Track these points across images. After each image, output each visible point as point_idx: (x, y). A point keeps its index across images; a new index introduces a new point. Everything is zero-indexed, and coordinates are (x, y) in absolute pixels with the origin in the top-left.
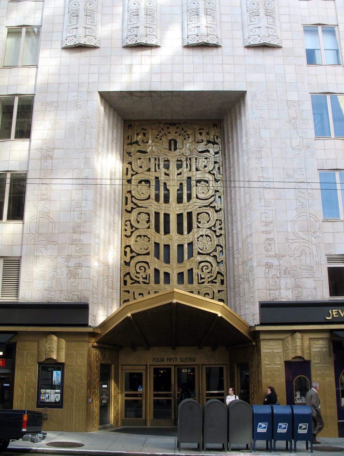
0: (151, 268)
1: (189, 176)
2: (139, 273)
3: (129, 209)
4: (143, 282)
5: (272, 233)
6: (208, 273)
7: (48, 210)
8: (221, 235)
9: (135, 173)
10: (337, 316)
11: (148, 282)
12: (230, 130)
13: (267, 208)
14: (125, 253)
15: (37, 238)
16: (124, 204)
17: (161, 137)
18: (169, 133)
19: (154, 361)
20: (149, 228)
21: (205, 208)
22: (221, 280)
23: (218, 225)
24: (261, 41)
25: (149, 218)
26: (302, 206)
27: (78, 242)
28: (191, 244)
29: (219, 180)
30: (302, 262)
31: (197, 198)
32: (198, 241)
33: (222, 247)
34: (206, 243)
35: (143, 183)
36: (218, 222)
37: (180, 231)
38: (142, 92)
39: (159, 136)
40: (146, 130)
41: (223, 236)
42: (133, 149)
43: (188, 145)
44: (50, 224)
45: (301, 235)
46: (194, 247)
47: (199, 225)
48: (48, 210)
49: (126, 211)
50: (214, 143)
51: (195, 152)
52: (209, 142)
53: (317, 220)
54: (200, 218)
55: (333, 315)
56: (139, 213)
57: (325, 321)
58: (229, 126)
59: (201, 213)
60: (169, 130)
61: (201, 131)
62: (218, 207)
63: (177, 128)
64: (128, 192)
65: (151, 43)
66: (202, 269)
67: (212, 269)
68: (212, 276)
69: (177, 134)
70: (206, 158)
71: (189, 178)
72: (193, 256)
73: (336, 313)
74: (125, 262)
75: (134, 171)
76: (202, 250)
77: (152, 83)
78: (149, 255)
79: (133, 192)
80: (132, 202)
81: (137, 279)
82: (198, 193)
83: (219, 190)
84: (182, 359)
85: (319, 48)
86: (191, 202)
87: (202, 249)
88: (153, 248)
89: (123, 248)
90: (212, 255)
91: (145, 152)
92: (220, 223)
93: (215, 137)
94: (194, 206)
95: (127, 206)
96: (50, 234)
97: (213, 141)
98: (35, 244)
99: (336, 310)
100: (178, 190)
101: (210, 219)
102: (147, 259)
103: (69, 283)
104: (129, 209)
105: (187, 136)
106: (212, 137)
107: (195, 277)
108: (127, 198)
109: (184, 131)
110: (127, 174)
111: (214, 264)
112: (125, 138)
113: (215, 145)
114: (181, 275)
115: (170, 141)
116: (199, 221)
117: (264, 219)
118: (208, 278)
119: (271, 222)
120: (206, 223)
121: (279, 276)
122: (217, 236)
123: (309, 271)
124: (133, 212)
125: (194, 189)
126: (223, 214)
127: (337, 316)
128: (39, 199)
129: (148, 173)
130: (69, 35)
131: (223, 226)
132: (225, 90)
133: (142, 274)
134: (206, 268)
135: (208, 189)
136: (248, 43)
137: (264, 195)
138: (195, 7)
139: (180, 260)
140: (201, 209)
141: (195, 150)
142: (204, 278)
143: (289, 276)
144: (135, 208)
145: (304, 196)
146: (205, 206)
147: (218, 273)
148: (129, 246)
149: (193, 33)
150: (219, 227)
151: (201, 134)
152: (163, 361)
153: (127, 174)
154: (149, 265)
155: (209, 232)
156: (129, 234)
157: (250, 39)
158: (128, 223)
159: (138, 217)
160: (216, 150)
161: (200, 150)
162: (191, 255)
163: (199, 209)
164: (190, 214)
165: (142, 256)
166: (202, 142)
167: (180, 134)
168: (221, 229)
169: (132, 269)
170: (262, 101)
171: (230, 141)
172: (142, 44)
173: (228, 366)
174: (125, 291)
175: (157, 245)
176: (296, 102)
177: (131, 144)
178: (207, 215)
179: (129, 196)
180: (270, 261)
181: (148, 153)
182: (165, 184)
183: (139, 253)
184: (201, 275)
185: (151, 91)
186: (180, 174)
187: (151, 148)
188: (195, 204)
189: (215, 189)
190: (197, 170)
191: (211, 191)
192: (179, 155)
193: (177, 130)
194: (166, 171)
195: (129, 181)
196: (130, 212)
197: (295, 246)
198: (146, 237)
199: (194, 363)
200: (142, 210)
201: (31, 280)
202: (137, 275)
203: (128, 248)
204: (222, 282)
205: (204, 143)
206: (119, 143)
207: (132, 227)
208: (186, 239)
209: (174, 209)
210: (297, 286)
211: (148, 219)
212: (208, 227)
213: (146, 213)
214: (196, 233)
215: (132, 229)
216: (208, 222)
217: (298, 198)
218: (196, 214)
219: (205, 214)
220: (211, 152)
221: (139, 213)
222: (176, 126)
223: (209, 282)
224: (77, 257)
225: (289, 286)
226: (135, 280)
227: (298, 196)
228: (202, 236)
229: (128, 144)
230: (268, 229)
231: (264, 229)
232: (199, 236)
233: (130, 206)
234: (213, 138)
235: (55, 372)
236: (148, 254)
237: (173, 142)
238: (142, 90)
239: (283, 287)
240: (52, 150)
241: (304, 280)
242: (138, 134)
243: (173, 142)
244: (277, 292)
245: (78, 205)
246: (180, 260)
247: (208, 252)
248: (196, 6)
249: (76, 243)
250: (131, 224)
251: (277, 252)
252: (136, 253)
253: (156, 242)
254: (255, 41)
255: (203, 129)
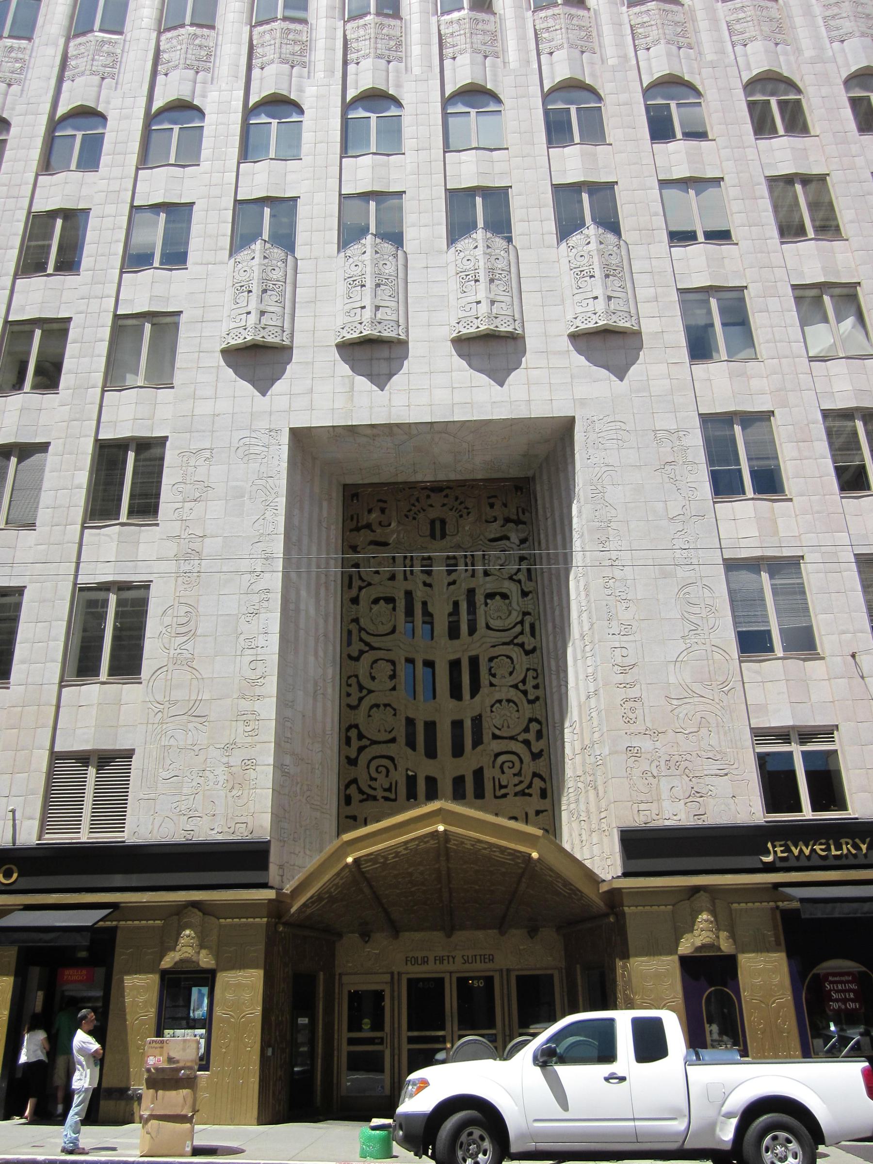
0: (399, 769)
1: (472, 586)
2: (376, 780)
3: (355, 654)
5: (638, 686)
6: (515, 775)
10: (785, 855)
11: (393, 796)
18: (431, 506)
19: (409, 963)
20: (394, 689)
21: (505, 647)
22: (541, 788)
25: (394, 671)
27: (250, 717)
28: (477, 721)
29: (530, 592)
30: (702, 743)
31: (488, 627)
32: (492, 711)
33: (539, 723)
34: (509, 714)
35: (382, 602)
36: (531, 674)
37: (456, 693)
39: (412, 513)
40: (385, 502)
43: (467, 528)
44: (195, 682)
46: (485, 725)
50: (518, 522)
52: (507, 520)
55: (775, 852)
56: (375, 662)
57: (761, 866)
58: (546, 487)
59: (497, 657)
60: (430, 502)
62: (529, 645)
63: (446, 496)
64: (353, 621)
66: (501, 767)
67: (521, 768)
68: (521, 782)
69: (445, 508)
71: (471, 592)
72: (482, 743)
73: (782, 848)
74: (347, 758)
75: (363, 581)
77: (392, 408)
79: (362, 622)
80: (361, 640)
81: (372, 792)
82: (489, 618)
83: (530, 610)
84: (466, 958)
86: (476, 636)
88: (403, 730)
89: (343, 730)
90: (520, 738)
91: (385, 544)
92: (535, 675)
93: (520, 510)
94: (479, 645)
96: (193, 702)
97: (515, 517)
99: (782, 843)
100: (450, 615)
102: (391, 750)
103: (230, 799)
104: (355, 654)
106: (514, 510)
107: (488, 786)
108: (350, 632)
109: (459, 501)
110: (350, 586)
111: (527, 758)
113: (520, 526)
114: (459, 782)
115: (433, 522)
117: (619, 660)
118: (515, 785)
120: (507, 675)
122: (530, 702)
125: (481, 610)
126: (540, 657)
127: (785, 855)
133: (382, 781)
134: (511, 765)
136: (574, 326)
138: (471, 265)
139: (458, 751)
140: (496, 648)
141: (482, 537)
142: (506, 787)
143: (677, 772)
144: (367, 652)
146: (504, 644)
147: (535, 775)
148: (356, 726)
150: (534, 682)
151: (492, 506)
152: (427, 962)
153: (350, 586)
155: (513, 694)
158: (353, 681)
159: (372, 668)
160: (522, 535)
161: (492, 536)
162: (478, 741)
163: (492, 649)
164: (474, 662)
166: (495, 520)
168: (536, 687)
169: (360, 773)
172: (372, 337)
173: (564, 971)
175: (410, 722)
177: (358, 529)
178: (508, 660)
179: (354, 627)
182: (425, 604)
183: (374, 739)
187: (395, 536)
191: (514, 614)
193: (446, 501)
194: (425, 577)
195: (355, 601)
196: (357, 659)
197: (685, 712)
199: (490, 966)
202: (373, 784)
204: (543, 794)
205: (500, 522)
207: (361, 688)
209: (444, 651)
211: (392, 673)
212: (511, 683)
213: (387, 661)
215: (361, 691)
216: (511, 673)
218: (486, 659)
219: (504, 658)
220: (512, 540)
221: (375, 662)
222: (444, 493)
223: (516, 794)
224: (247, 745)
228: (500, 701)
229: (351, 530)
230: (629, 678)
232: (493, 702)
233: (357, 646)
235: (195, 990)
236: (393, 740)
237: (438, 525)
239: (665, 794)
242: (370, 511)
243: (438, 525)
244: (654, 807)
246: (458, 751)
248: (472, 264)
251: (649, 725)
252: (369, 739)
255: (495, 496)
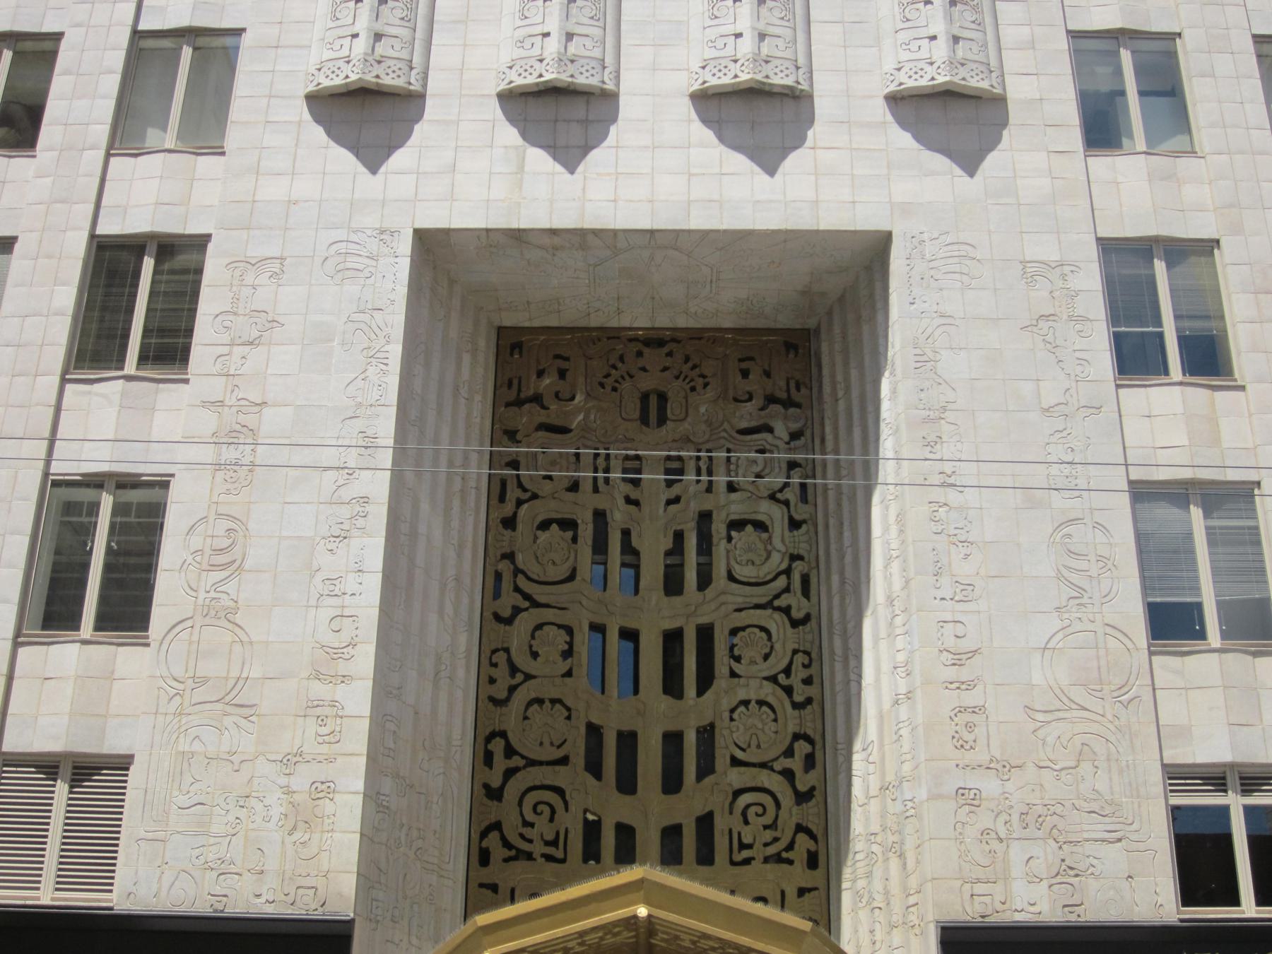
0: (572, 808)
1: (707, 507)
2: (532, 825)
4: (543, 855)
5: (980, 687)
6: (766, 827)
7: (232, 604)
8: (809, 701)
9: (528, 495)
11: (559, 854)
12: (839, 359)
14: (488, 759)
15: (188, 692)
16: (489, 593)
17: (616, 381)
18: (644, 369)
20: (569, 674)
22: (809, 851)
23: (801, 668)
24: (937, 77)
25: (571, 644)
27: (328, 711)
31: (731, 578)
32: (732, 719)
34: (760, 726)
35: (554, 527)
36: (800, 658)
37: (672, 685)
38: (553, 232)
40: (567, 359)
41: (815, 705)
42: (525, 418)
43: (702, 410)
45: (1079, 695)
46: (719, 741)
47: (735, 665)
48: (232, 604)
50: (789, 403)
51: (725, 430)
52: (771, 400)
54: (740, 644)
56: (539, 627)
59: (743, 629)
60: (641, 363)
61: (744, 365)
62: (799, 609)
63: (670, 354)
68: (776, 840)
71: (705, 518)
74: (486, 786)
75: (525, 490)
76: (743, 750)
78: (566, 764)
79: (520, 558)
80: (517, 589)
82: (733, 563)
83: (802, 552)
86: (710, 593)
87: (744, 746)
90: (778, 766)
92: (806, 662)
93: (792, 385)
94: (715, 607)
95: (498, 602)
97: (784, 395)
98: (180, 714)
100: (668, 553)
101: (772, 647)
102: (559, 776)
104: (506, 613)
105: (701, 380)
106: (783, 384)
107: (721, 843)
108: (498, 576)
109: (690, 364)
110: (502, 499)
111: (787, 799)
112: (499, 383)
113: (792, 410)
115: (645, 397)
116: (736, 652)
117: (950, 642)
118: (766, 845)
120: (759, 660)
121: (1002, 835)
122: (795, 706)
123: (1107, 820)
124: (517, 621)
126: (816, 632)
128: (205, 566)
129: (571, 495)
130: (329, 55)
131: (813, 670)
132: (821, 228)
133: (543, 828)
134: (760, 810)
135: (766, 549)
136: (896, 83)
137: (950, 564)
139: (672, 782)
142: (750, 846)
143: (1040, 834)
144: (526, 609)
146: (757, 607)
147: (800, 828)
148: (503, 734)
149: (722, 54)
151: (745, 374)
153: (502, 499)
154: (568, 797)
155: (768, 692)
156: (503, 695)
157: (903, 71)
158: (501, 658)
159: (533, 637)
160: (795, 426)
161: (744, 424)
164: (705, 634)
165: (544, 768)
166: (750, 399)
167: (676, 373)
168: (808, 681)
170: (943, 262)
171: (840, 394)
174: (481, 885)
175: (594, 731)
177: (519, 403)
178: (763, 635)
180: (972, 781)
181: (571, 434)
182: (626, 533)
183: (532, 756)
184: (739, 834)
186: (677, 500)
187: (581, 417)
188: (723, 598)
189: (791, 551)
190: (731, 488)
191: (776, 557)
192: (674, 441)
193: (668, 362)
196: (509, 621)
198: (558, 706)
200: (549, 615)
201: (161, 835)
202: (527, 832)
203: (498, 739)
205: (758, 402)
206: (478, 398)
207: (514, 669)
208: (692, 712)
209: (656, 615)
210: (1067, 871)
211: (566, 647)
212: (766, 674)
213: (560, 626)
214: (723, 693)
215: (513, 675)
216: (766, 657)
217: (1065, 572)
219: (756, 630)
220: (777, 432)
221: (539, 627)
222: (666, 350)
223: (766, 860)
225: (1039, 866)
226: (518, 850)
227: (1065, 566)
228: (746, 703)
229: (508, 405)
230: (965, 674)
231: (951, 673)
233: (509, 600)
234: (785, 388)
236: (564, 761)
237: (653, 401)
238: (554, 227)
239: (1017, 870)
240: (257, 409)
241: (1089, 848)
242: (540, 374)
243: (653, 401)
244: (998, 891)
245: (332, 587)
246: (672, 782)
247: (765, 758)
249: (318, 711)
250: (510, 660)
252: (523, 757)
253: (594, 721)
254: (916, 76)
255: (751, 359)
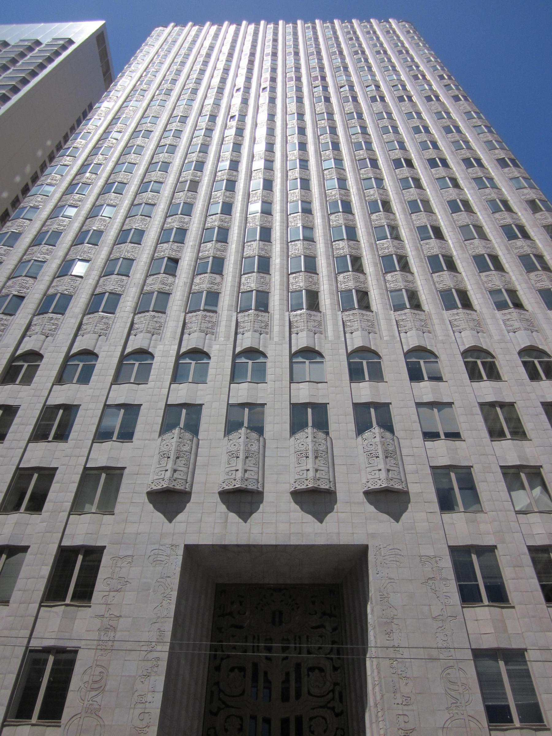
13: (406, 708)
25: (242, 725)
26: (455, 705)
31: (309, 693)
35: (236, 670)
38: (238, 546)
48: (98, 707)
49: (211, 713)
52: (324, 614)
53: (480, 726)
56: (228, 717)
59: (315, 718)
65: (252, 488)
70: (321, 636)
80: (220, 699)
85: (421, 410)
91: (241, 627)
100: (283, 682)
108: (212, 693)
117: (403, 725)
119: (413, 729)
128: (89, 689)
136: (367, 487)
145: (456, 688)
151: (314, 603)
164: (299, 720)
166: (316, 613)
176: (432, 557)
182: (266, 673)
185: (249, 545)
195: (218, 668)
196: (216, 714)
221: (228, 717)
242: (232, 603)
